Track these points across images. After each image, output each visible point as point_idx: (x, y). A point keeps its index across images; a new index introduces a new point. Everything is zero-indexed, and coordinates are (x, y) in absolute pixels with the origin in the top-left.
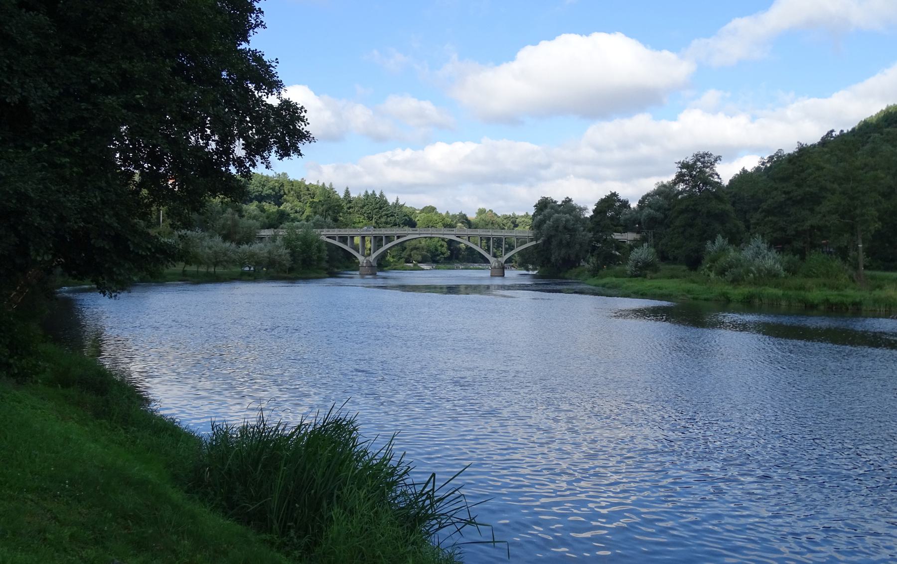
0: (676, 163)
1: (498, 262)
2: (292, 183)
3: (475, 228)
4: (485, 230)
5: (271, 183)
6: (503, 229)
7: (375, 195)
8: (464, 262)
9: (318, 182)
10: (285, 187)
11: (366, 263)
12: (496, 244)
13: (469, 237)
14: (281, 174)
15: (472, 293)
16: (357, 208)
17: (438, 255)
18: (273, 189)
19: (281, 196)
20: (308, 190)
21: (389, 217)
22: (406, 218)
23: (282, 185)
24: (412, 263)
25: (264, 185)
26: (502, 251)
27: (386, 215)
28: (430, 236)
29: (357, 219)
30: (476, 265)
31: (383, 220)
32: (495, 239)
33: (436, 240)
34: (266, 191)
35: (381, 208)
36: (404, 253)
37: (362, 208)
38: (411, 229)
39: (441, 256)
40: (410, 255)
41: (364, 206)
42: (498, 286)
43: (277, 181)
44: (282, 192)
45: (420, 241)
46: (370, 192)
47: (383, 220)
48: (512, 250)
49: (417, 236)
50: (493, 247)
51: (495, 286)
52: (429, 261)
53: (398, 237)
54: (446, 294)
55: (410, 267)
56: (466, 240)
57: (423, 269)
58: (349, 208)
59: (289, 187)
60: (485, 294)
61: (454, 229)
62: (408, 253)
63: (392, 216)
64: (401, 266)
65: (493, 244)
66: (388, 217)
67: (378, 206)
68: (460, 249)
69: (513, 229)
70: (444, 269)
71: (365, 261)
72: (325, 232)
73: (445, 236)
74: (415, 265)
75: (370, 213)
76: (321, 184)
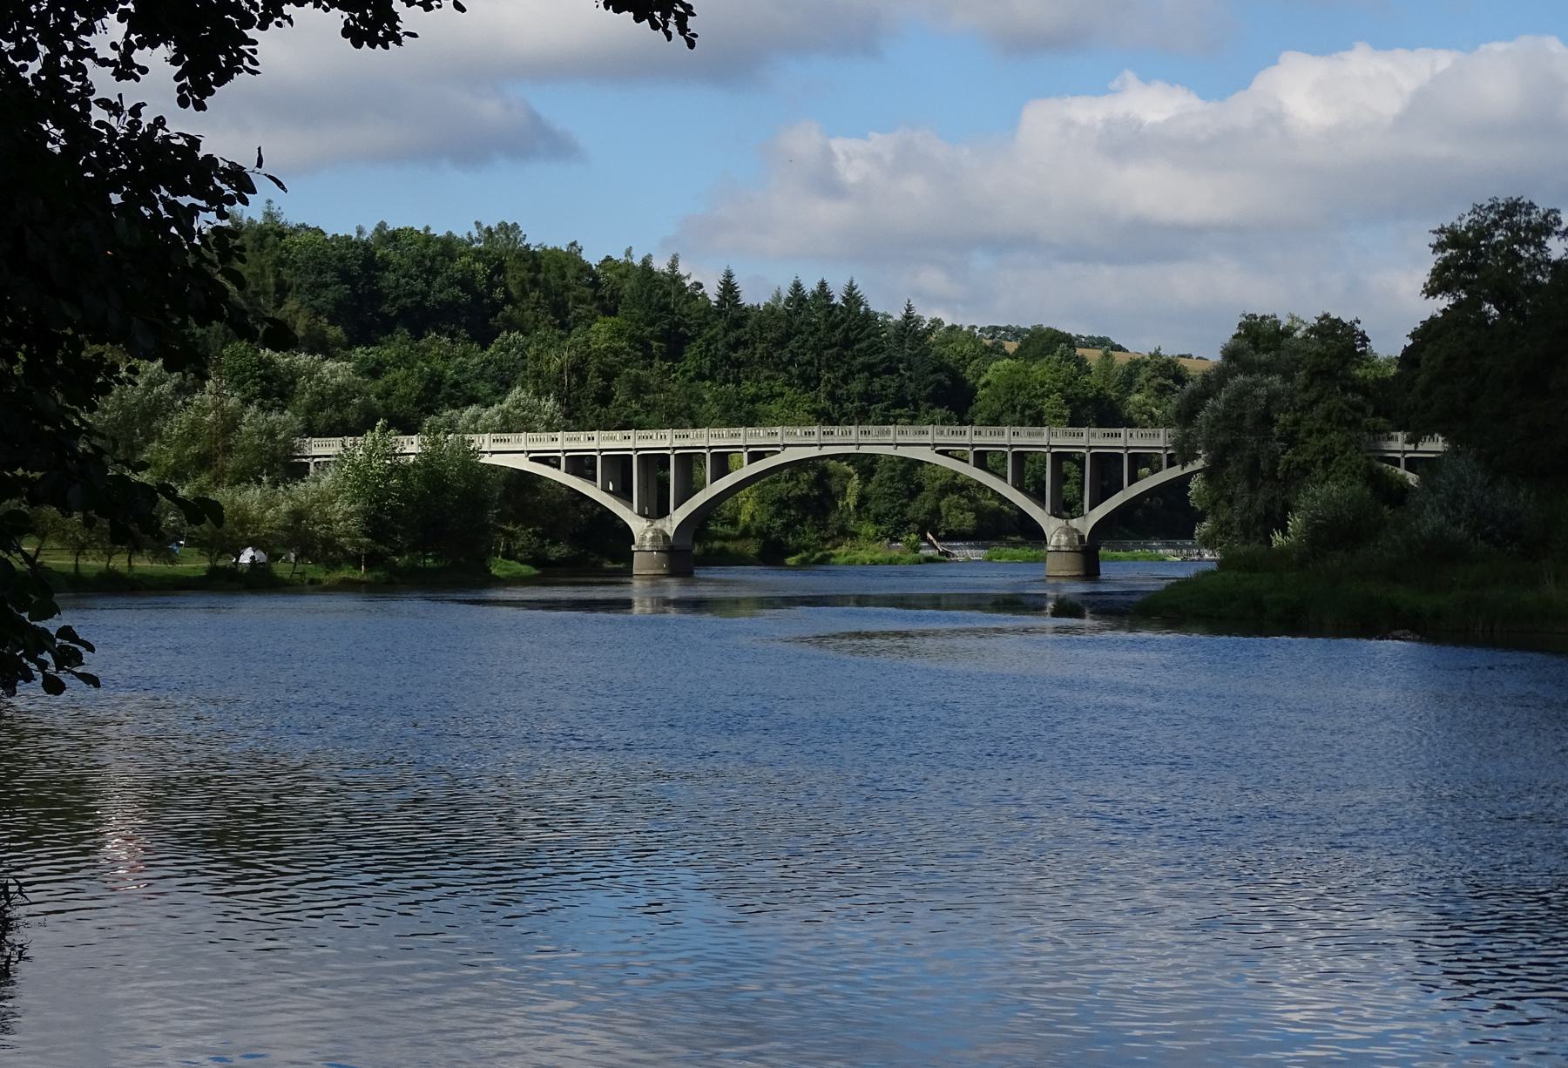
0: (1435, 232)
2: (534, 261)
5: (459, 264)
7: (829, 297)
9: (628, 253)
10: (509, 275)
11: (653, 539)
14: (494, 226)
16: (760, 347)
18: (466, 283)
19: (496, 307)
20: (595, 284)
21: (878, 375)
22: (942, 376)
23: (500, 269)
25: (433, 272)
27: (868, 367)
29: (764, 384)
31: (857, 386)
34: (439, 291)
35: (847, 344)
36: (916, 504)
37: (781, 343)
40: (935, 512)
41: (788, 337)
43: (479, 255)
44: (498, 294)
46: (810, 287)
47: (857, 386)
53: (755, 457)
58: (734, 347)
59: (524, 274)
63: (891, 370)
66: (873, 375)
67: (838, 335)
71: (649, 535)
72: (523, 441)
75: (810, 363)
76: (637, 262)
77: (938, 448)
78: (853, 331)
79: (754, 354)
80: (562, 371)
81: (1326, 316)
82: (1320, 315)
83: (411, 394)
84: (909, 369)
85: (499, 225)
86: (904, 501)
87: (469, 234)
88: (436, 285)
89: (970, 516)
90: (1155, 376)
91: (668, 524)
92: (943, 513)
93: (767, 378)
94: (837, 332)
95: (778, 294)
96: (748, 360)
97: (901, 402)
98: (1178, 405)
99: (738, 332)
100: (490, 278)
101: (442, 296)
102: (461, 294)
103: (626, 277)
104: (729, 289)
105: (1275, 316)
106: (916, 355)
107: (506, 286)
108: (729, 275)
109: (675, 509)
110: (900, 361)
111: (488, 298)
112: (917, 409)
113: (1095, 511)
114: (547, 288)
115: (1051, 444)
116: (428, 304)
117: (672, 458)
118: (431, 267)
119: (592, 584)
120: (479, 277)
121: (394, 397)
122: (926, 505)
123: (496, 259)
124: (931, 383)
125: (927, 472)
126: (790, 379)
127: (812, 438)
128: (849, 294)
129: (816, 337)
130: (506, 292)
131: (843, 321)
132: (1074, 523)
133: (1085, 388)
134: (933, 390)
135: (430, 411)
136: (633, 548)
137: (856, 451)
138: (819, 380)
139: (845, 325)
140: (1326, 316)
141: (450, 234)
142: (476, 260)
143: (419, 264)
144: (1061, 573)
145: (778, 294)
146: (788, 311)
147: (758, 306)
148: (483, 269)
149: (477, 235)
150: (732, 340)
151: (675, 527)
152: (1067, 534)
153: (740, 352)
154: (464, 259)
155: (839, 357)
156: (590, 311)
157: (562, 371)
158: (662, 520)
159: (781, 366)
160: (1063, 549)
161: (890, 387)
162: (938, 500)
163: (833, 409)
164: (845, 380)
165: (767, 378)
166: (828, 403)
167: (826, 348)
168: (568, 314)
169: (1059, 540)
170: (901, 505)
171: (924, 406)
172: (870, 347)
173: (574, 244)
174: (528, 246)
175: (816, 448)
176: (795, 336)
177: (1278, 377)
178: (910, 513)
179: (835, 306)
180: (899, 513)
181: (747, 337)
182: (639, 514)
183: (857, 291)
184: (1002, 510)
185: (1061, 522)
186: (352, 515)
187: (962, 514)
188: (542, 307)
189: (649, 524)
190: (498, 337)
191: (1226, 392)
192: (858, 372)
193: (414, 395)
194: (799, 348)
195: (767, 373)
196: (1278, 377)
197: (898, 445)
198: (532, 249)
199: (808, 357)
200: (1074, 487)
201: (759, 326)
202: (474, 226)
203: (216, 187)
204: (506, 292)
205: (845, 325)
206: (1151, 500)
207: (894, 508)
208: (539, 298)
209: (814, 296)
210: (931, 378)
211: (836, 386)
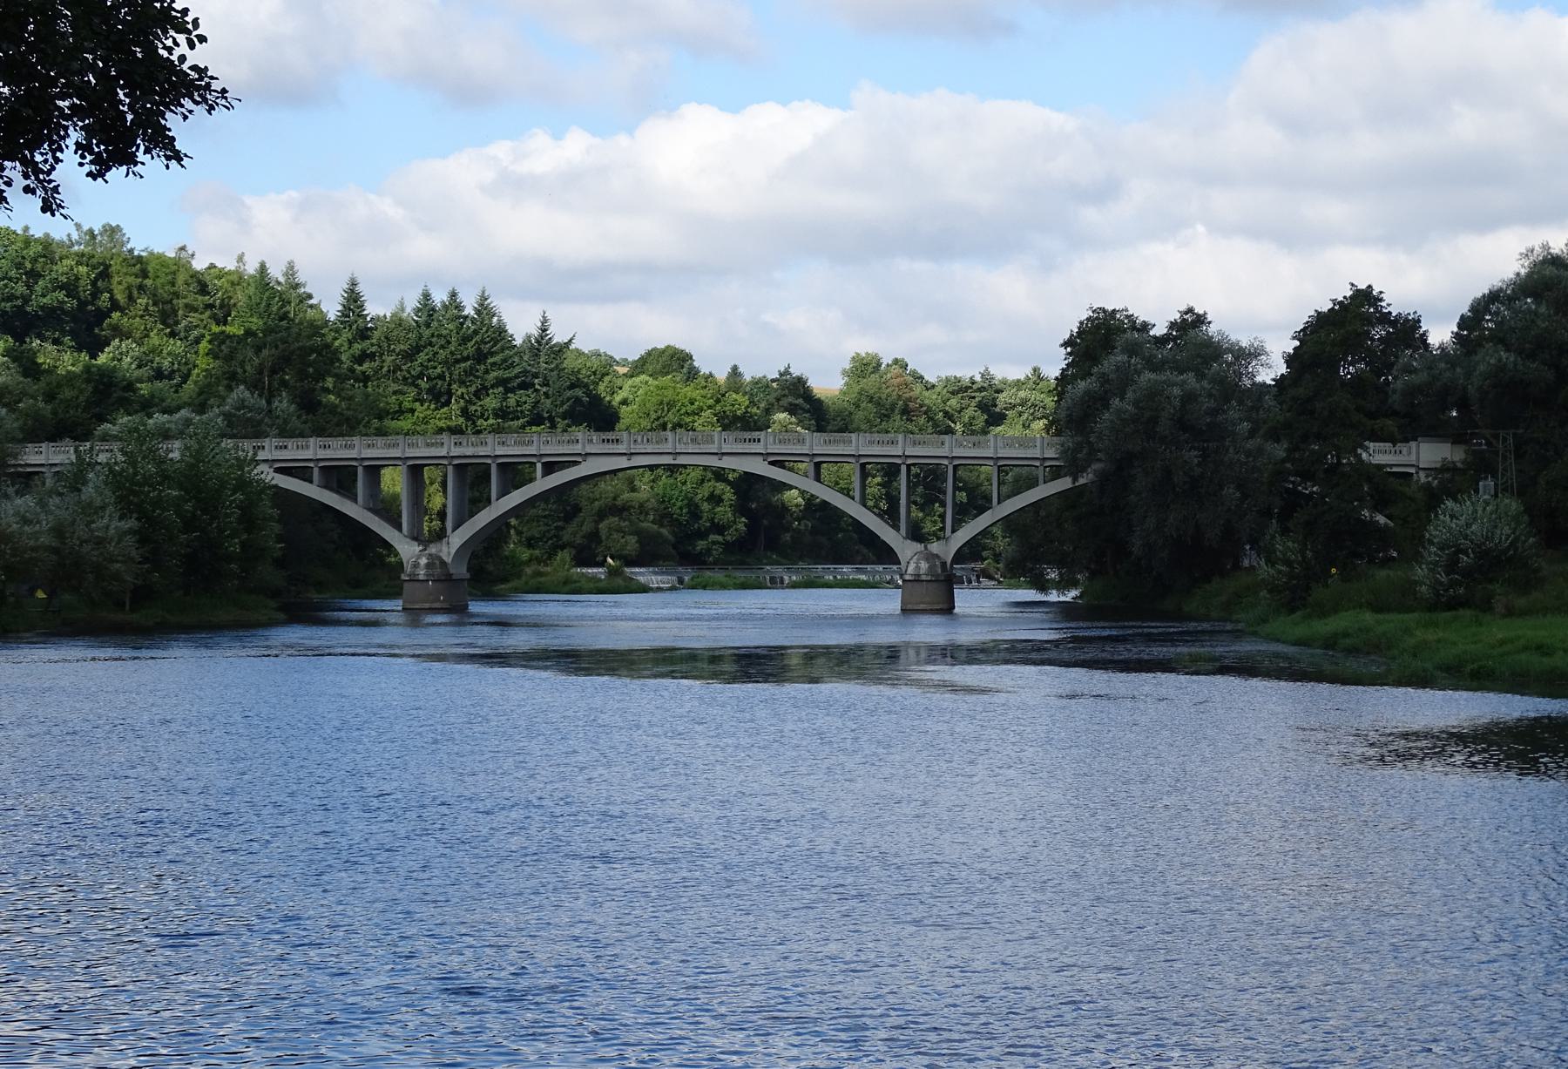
2: (141, 265)
7: (459, 307)
9: (240, 259)
10: (116, 279)
11: (428, 566)
18: (70, 287)
19: (103, 315)
20: (203, 289)
21: (513, 390)
22: (579, 392)
23: (105, 274)
25: (34, 275)
27: (501, 382)
31: (491, 402)
34: (44, 297)
35: (480, 357)
36: (572, 528)
41: (417, 349)
43: (81, 258)
46: (439, 297)
53: (550, 468)
59: (131, 279)
63: (525, 386)
66: (507, 390)
71: (423, 561)
75: (441, 377)
77: (771, 459)
78: (486, 343)
79: (382, 367)
80: (261, 372)
81: (1190, 311)
82: (1184, 308)
83: (77, 397)
84: (545, 384)
85: (104, 227)
86: (559, 524)
87: (69, 235)
88: (38, 288)
89: (632, 540)
90: (784, 396)
91: (445, 549)
93: (395, 393)
94: (470, 344)
95: (402, 304)
96: (376, 372)
97: (537, 420)
98: (1068, 409)
99: (364, 345)
100: (94, 283)
101: (45, 301)
102: (66, 299)
103: (238, 284)
104: (353, 300)
105: (1127, 310)
106: (552, 370)
107: (110, 291)
108: (354, 283)
109: (454, 529)
110: (536, 376)
111: (93, 305)
112: (553, 426)
113: (959, 533)
114: (155, 295)
116: (29, 309)
117: (360, 471)
118: (32, 270)
120: (82, 282)
121: (57, 401)
122: (584, 528)
123: (101, 264)
124: (568, 399)
126: (419, 394)
127: (620, 446)
128: (481, 305)
129: (448, 351)
130: (112, 299)
131: (476, 332)
132: (935, 547)
133: (733, 405)
134: (570, 406)
135: (101, 419)
136: (404, 577)
137: (673, 462)
138: (450, 394)
139: (478, 338)
140: (1190, 311)
141: (47, 235)
142: (79, 263)
143: (19, 266)
144: (922, 606)
145: (402, 304)
146: (417, 322)
147: (385, 316)
148: (88, 273)
149: (77, 238)
150: (358, 353)
151: (453, 551)
152: (927, 560)
153: (366, 365)
154: (65, 262)
155: (470, 372)
156: (202, 320)
157: (261, 372)
158: (439, 545)
159: (410, 380)
160: (924, 578)
161: (525, 403)
162: (597, 522)
163: (466, 426)
164: (477, 394)
165: (395, 393)
166: (462, 420)
167: (457, 361)
168: (177, 323)
169: (918, 568)
171: (561, 424)
172: (505, 361)
173: (183, 248)
174: (131, 251)
175: (625, 458)
176: (425, 347)
177: (1191, 374)
178: (566, 537)
179: (466, 317)
180: (555, 536)
181: (374, 349)
183: (489, 301)
184: (660, 535)
185: (919, 547)
186: (125, 533)
187: (623, 537)
188: (151, 315)
189: (421, 548)
190: (109, 345)
191: (1134, 391)
192: (492, 387)
193: (81, 398)
194: (429, 360)
195: (395, 387)
196: (1191, 374)
197: (724, 454)
198: (136, 253)
199: (439, 370)
200: (728, 509)
201: (386, 338)
202: (74, 228)
203: (89, 80)
204: (112, 299)
205: (478, 338)
207: (548, 531)
208: (147, 304)
209: (445, 307)
210: (569, 393)
211: (470, 402)
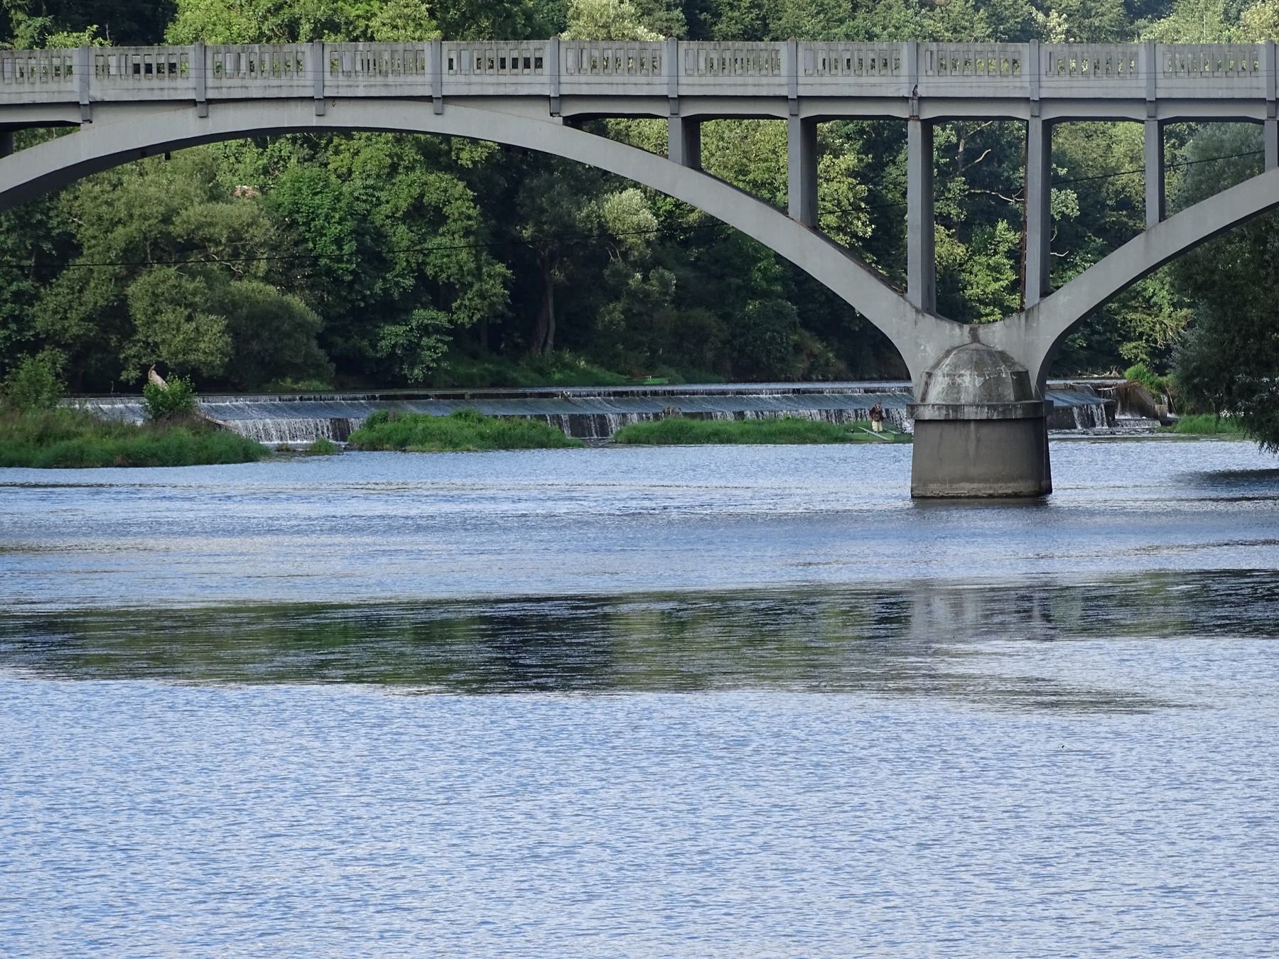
1: (987, 360)
3: (750, 35)
4: (843, 50)
6: (1028, 33)
8: (650, 367)
12: (957, 185)
13: (692, 126)
15: (733, 676)
17: (393, 310)
24: (137, 388)
26: (1016, 255)
28: (303, 117)
30: (214, 605)
32: (942, 135)
33: (374, 154)
36: (55, 296)
38: (115, 57)
39: (422, 315)
42: (993, 596)
45: (209, 174)
48: (1118, 237)
49: (186, 124)
50: (932, 218)
51: (956, 597)
52: (299, 372)
54: (480, 683)
55: (107, 428)
56: (661, 151)
57: (246, 453)
60: (858, 683)
61: (546, 49)
62: (98, 295)
64: (33, 419)
65: (934, 181)
68: (607, 238)
69: (1125, 35)
70: (452, 443)
73: (456, 122)
74: (164, 411)
86: (26, 285)
89: (214, 325)
92: (139, 319)
115: (922, 92)
119: (694, 592)
122: (88, 296)
125: (89, 205)
137: (315, 122)
152: (978, 366)
160: (970, 413)
162: (121, 281)
169: (954, 387)
170: (18, 296)
182: (927, 309)
184: (287, 309)
185: (956, 333)
187: (189, 319)
197: (447, 99)
200: (459, 242)
206: (646, 279)
